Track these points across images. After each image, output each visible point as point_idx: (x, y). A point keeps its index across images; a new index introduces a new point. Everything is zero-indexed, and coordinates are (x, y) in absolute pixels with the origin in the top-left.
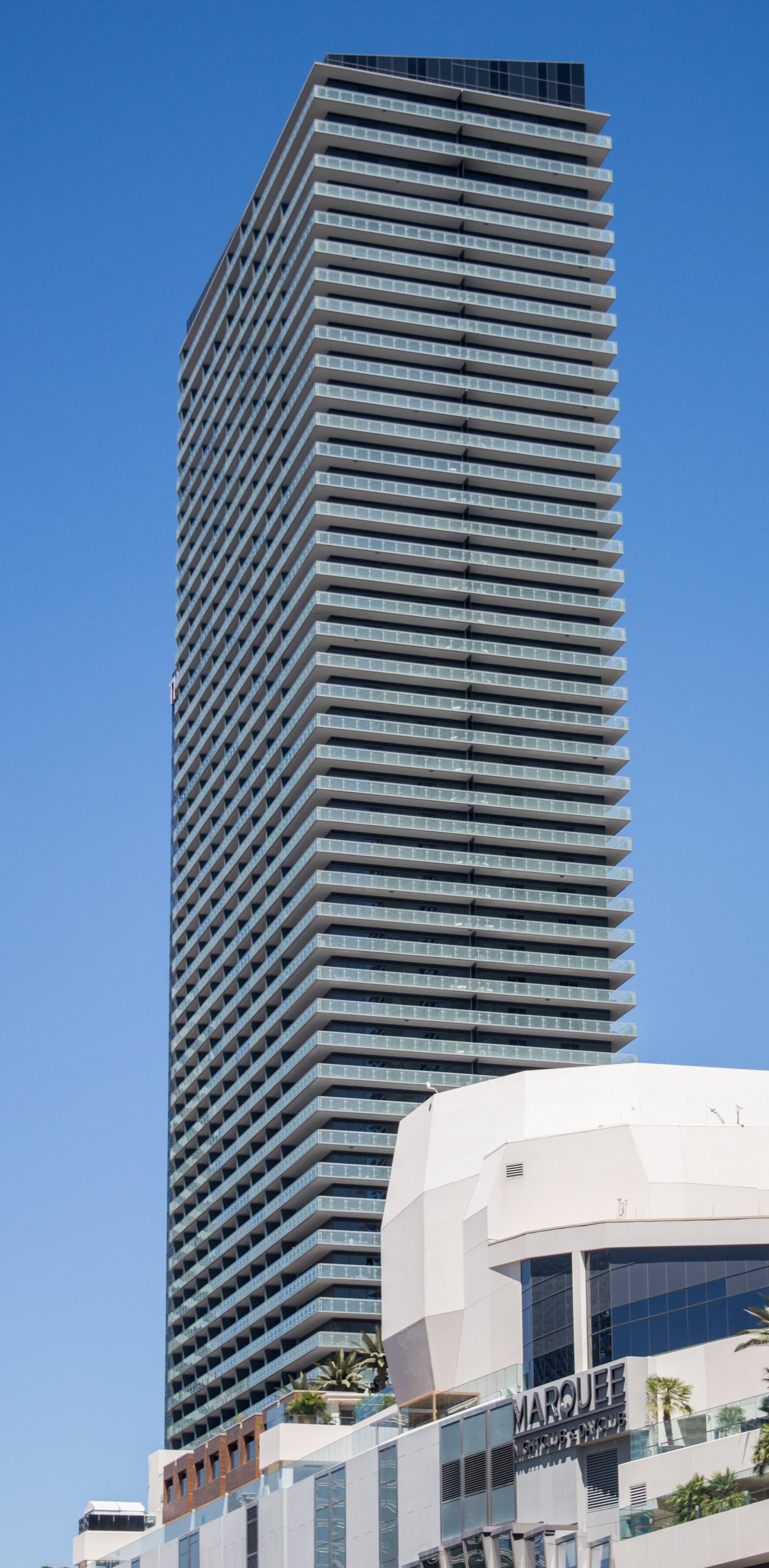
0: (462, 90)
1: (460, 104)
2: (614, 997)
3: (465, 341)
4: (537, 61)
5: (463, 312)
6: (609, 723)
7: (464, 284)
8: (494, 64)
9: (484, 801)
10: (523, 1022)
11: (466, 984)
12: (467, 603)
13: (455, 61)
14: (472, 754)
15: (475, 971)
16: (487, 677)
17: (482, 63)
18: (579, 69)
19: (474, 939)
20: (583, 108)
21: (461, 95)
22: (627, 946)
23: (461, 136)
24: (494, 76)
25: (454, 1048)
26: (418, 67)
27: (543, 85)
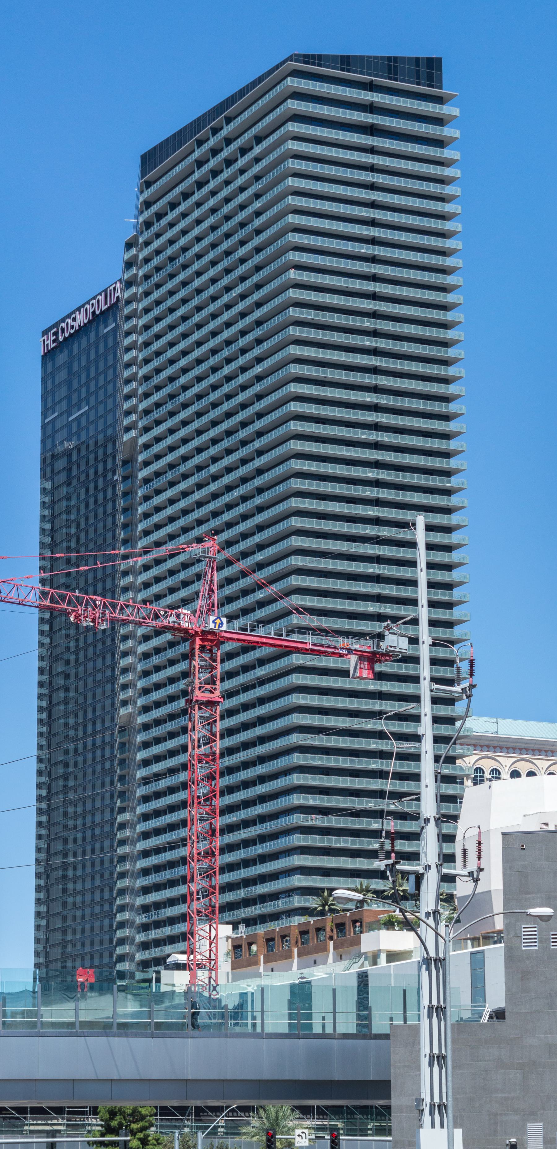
0: (373, 78)
1: (371, 87)
2: (450, 334)
3: (374, 241)
4: (414, 56)
5: (373, 223)
6: (450, 280)
7: (373, 205)
8: (389, 59)
9: (384, 381)
10: (404, 477)
11: (373, 472)
12: (376, 408)
13: (368, 57)
14: (374, 296)
15: (377, 465)
16: (387, 455)
17: (383, 58)
18: (439, 60)
19: (377, 446)
20: (441, 88)
21: (372, 81)
22: (458, 323)
23: (371, 108)
24: (389, 66)
25: (368, 606)
26: (345, 62)
27: (418, 72)
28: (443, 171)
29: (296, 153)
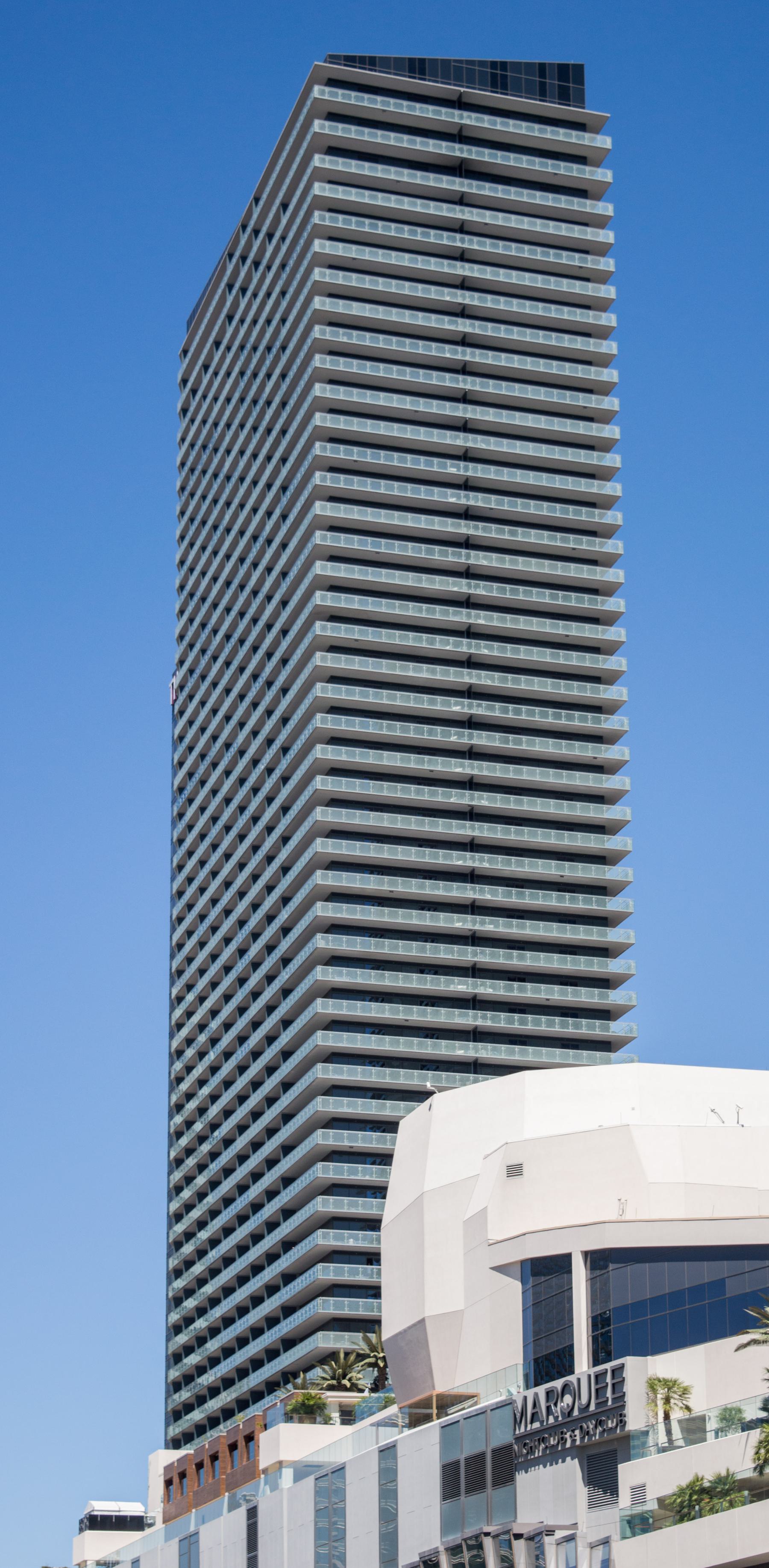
0: (462, 90)
1: (460, 104)
2: (614, 997)
3: (465, 341)
4: (537, 61)
5: (463, 312)
6: (609, 723)
7: (464, 284)
8: (494, 64)
9: (484, 801)
10: (523, 1022)
11: (466, 984)
12: (467, 603)
13: (455, 61)
14: (472, 754)
15: (475, 971)
16: (487, 677)
17: (482, 63)
18: (579, 69)
19: (474, 939)
20: (583, 108)
21: (461, 95)
22: (627, 946)
23: (461, 136)
24: (494, 76)
25: (454, 1048)
26: (418, 67)
27: (543, 85)
28: (598, 691)
29: (334, 614)
